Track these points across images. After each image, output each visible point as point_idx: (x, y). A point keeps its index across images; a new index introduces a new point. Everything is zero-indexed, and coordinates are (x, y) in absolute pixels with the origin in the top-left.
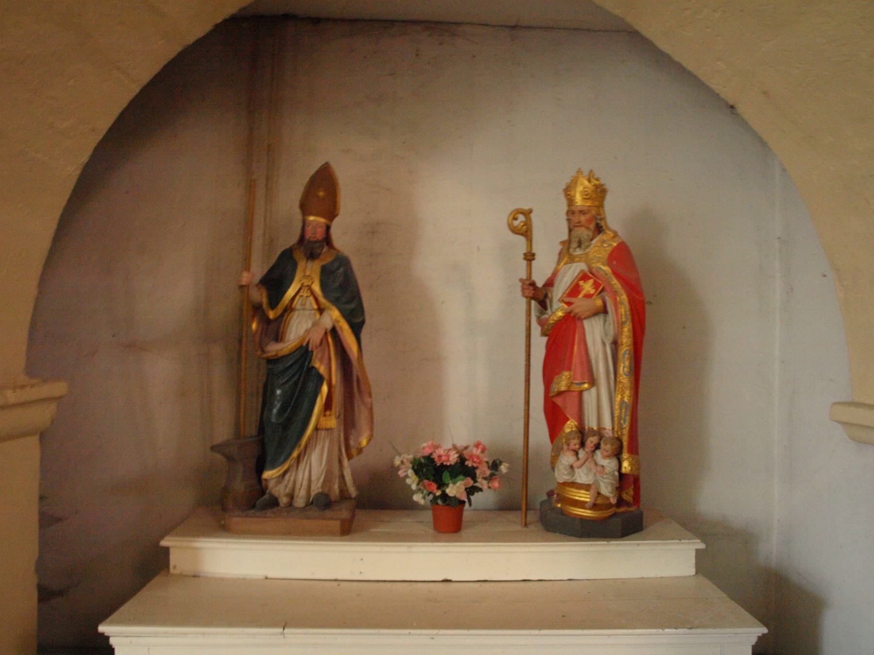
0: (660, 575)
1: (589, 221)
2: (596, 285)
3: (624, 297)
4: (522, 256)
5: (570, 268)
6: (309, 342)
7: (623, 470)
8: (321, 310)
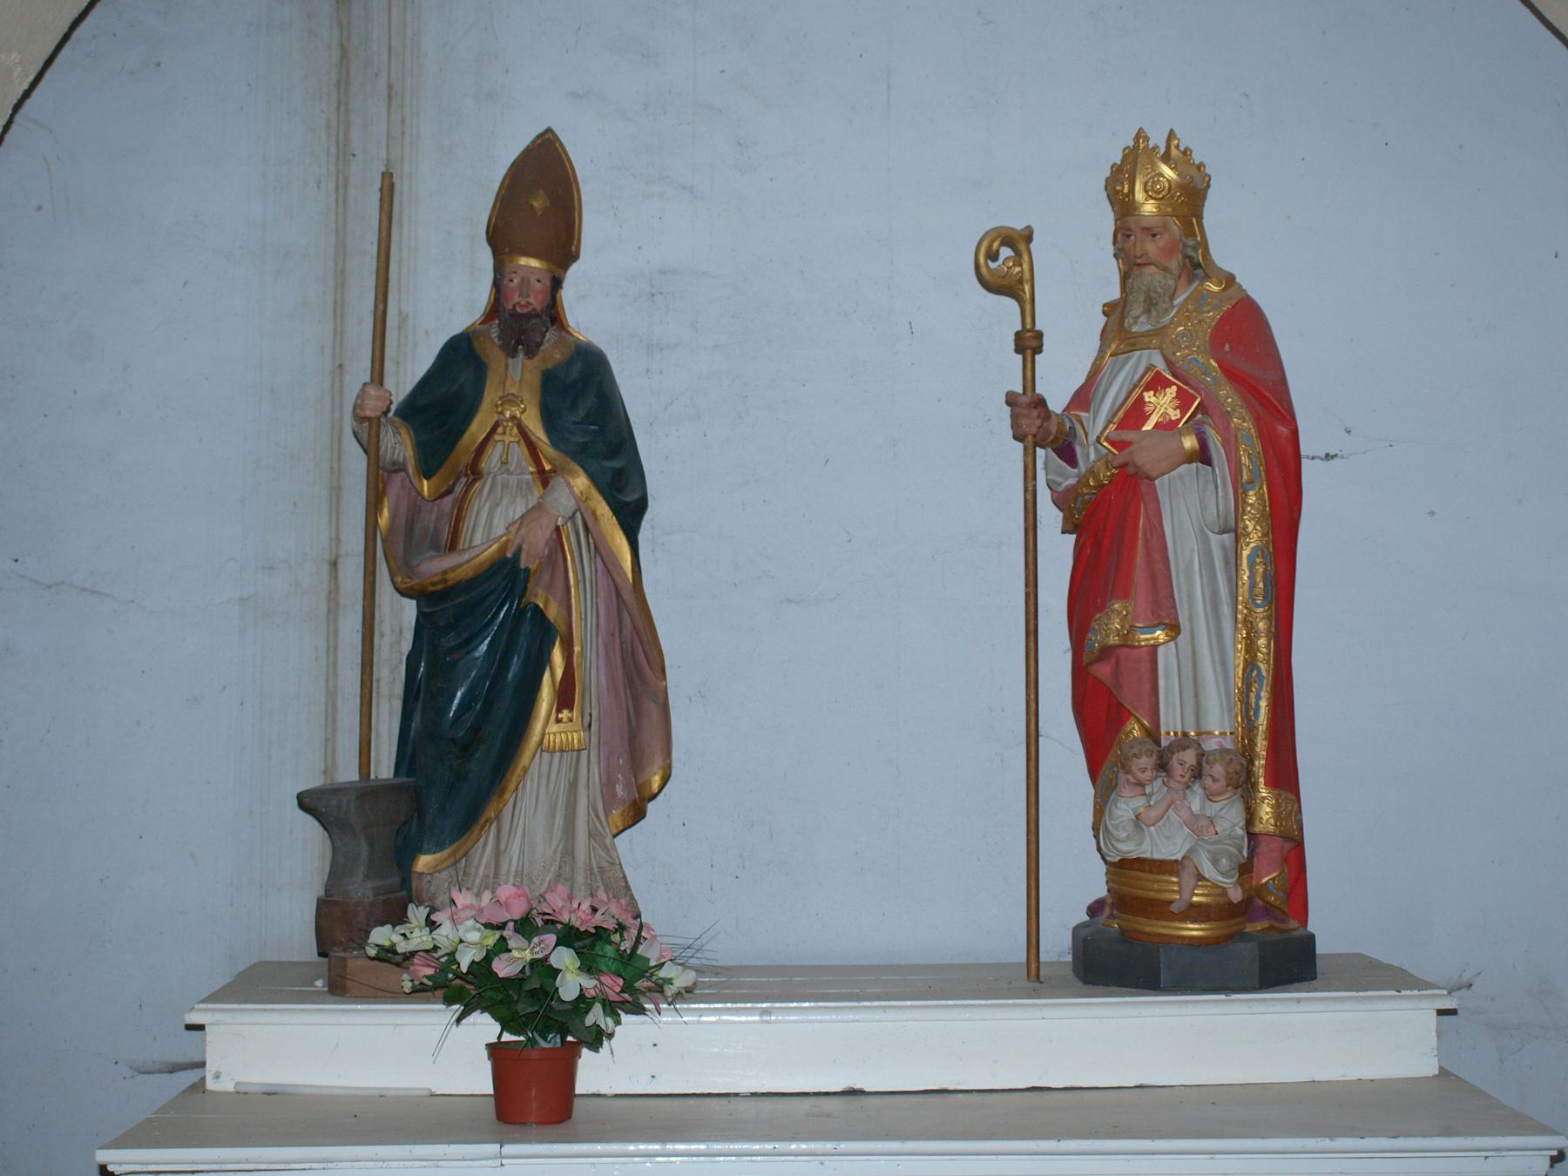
0: (1353, 1075)
1: (1169, 251)
2: (1183, 400)
3: (1248, 426)
4: (1085, 910)
5: (1126, 360)
6: (519, 549)
7: (1258, 828)
8: (544, 478)
